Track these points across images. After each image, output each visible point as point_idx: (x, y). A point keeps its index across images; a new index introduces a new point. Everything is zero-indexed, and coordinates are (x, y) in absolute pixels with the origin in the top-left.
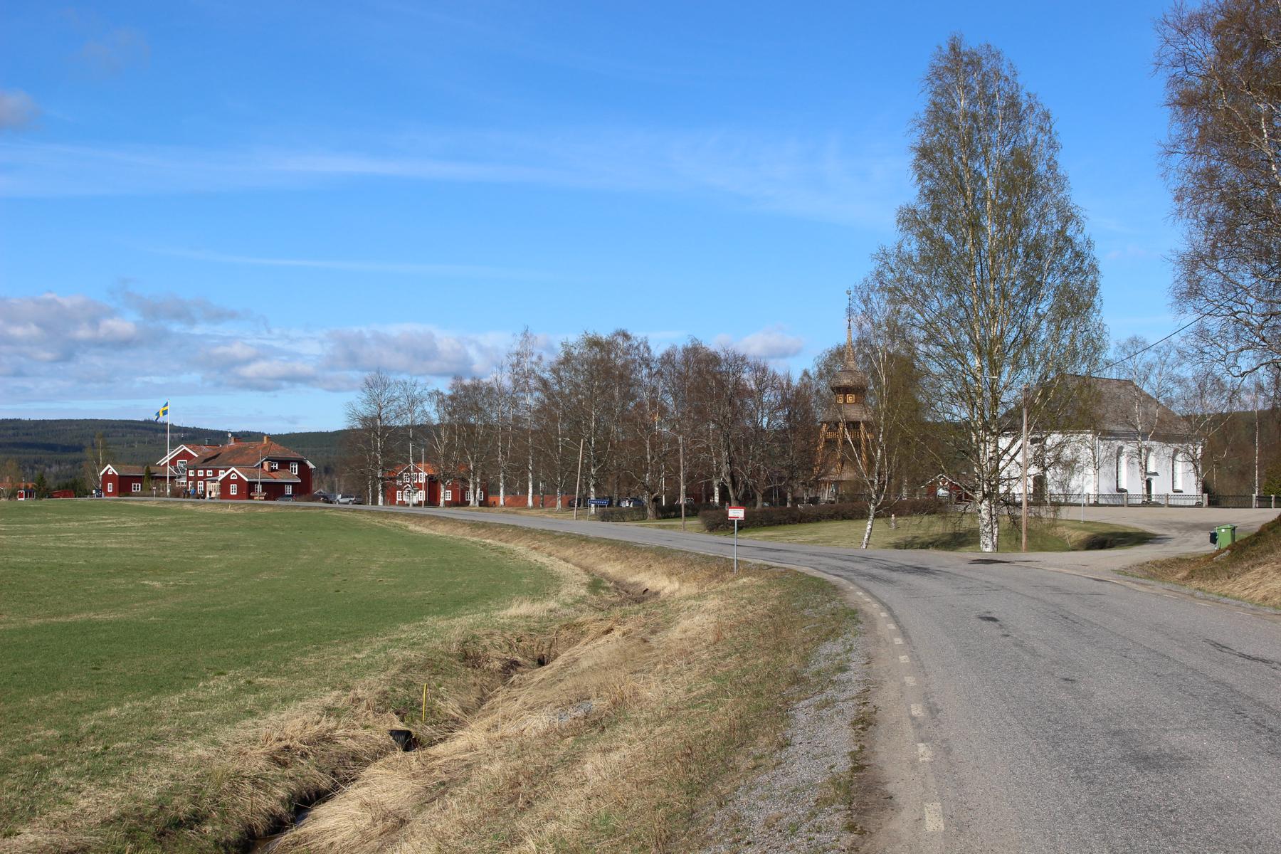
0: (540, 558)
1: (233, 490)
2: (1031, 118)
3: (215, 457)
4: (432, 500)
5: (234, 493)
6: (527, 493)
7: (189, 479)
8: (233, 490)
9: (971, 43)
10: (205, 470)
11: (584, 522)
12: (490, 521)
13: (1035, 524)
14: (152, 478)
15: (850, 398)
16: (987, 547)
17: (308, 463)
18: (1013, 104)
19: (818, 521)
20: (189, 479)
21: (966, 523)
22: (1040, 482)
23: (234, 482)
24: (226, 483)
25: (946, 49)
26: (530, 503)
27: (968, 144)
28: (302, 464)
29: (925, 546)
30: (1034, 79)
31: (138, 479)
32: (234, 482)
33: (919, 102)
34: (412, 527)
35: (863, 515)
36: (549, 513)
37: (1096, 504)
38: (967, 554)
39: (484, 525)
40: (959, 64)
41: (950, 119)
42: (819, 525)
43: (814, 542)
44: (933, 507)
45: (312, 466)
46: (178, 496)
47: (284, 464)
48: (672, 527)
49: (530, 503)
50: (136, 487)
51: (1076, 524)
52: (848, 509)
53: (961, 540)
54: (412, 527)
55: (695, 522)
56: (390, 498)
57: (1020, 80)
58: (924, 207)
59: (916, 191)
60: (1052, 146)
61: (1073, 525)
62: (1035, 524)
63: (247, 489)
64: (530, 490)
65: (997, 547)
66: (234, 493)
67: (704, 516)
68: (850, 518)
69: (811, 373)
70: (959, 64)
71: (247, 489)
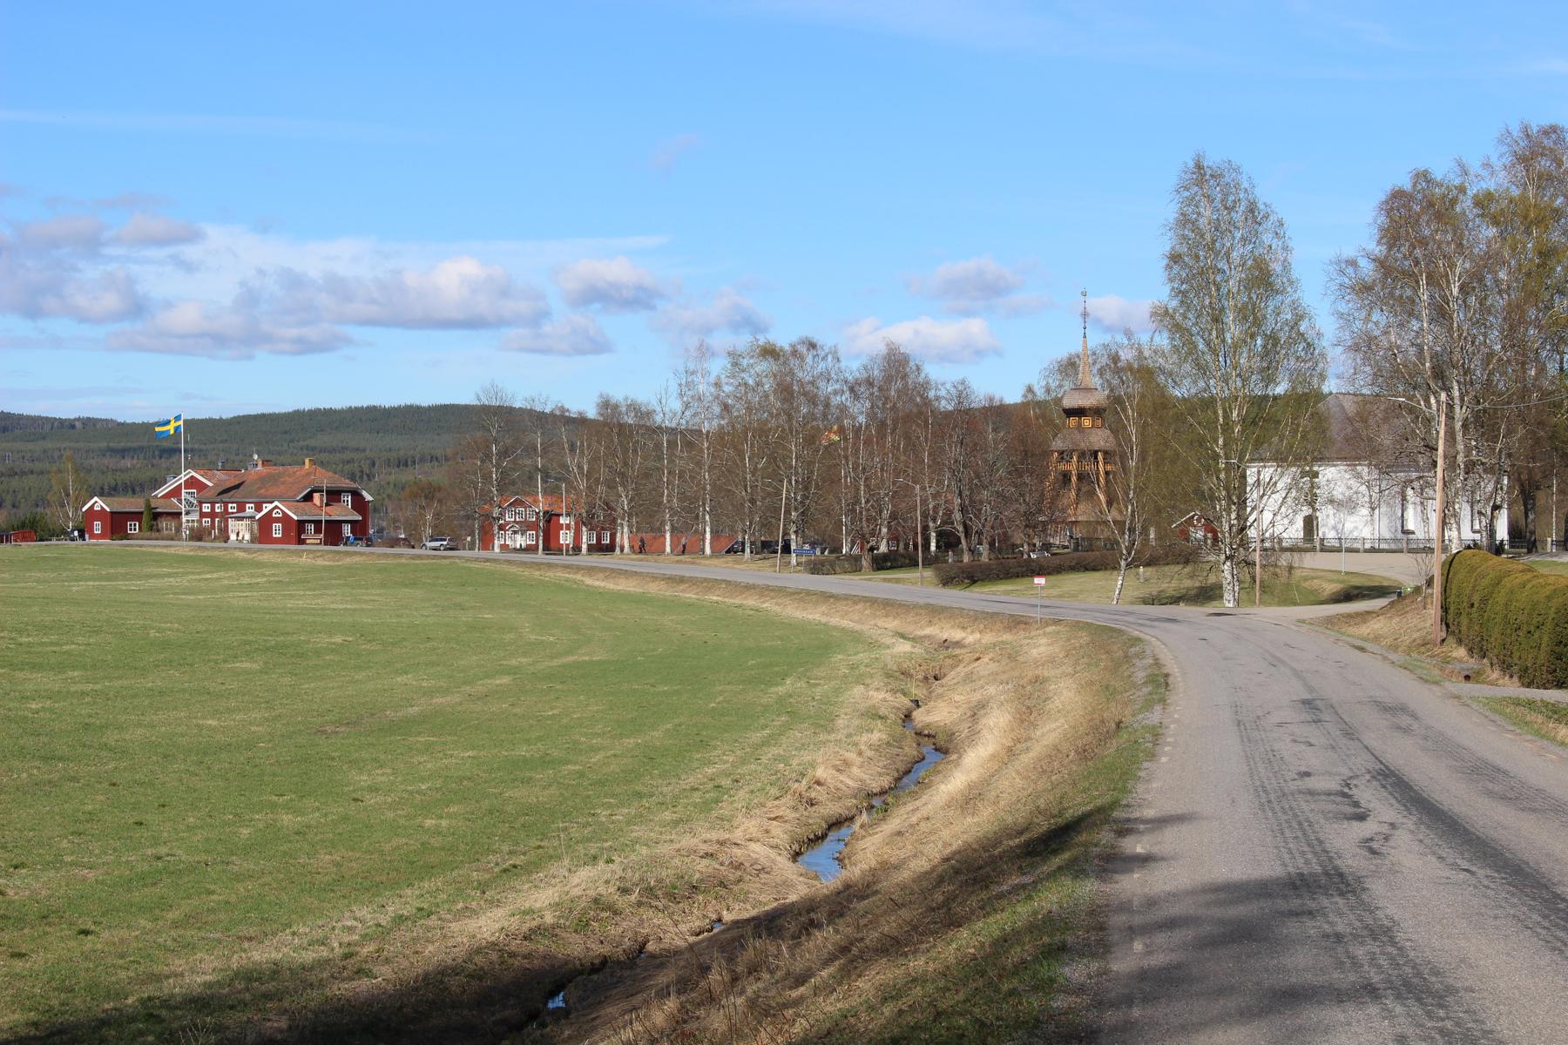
0: (814, 615)
1: (277, 531)
2: (1268, 224)
3: (237, 487)
4: (550, 545)
5: (277, 534)
6: (704, 540)
7: (203, 515)
8: (277, 531)
9: (1212, 160)
10: (213, 504)
11: (786, 575)
12: (687, 575)
13: (1271, 576)
14: (154, 519)
15: (1087, 422)
16: (1228, 602)
17: (364, 493)
18: (1252, 209)
19: (1059, 572)
20: (203, 515)
21: (1212, 579)
22: (1310, 524)
23: (277, 520)
24: (266, 522)
25: (1191, 164)
26: (708, 550)
27: (1211, 247)
28: (356, 494)
29: (1175, 600)
30: (1269, 188)
31: (136, 516)
32: (277, 520)
33: (1168, 210)
34: (588, 581)
35: (1116, 567)
36: (737, 562)
37: (1373, 550)
38: (1210, 608)
39: (682, 580)
40: (1200, 174)
41: (1196, 229)
42: (1060, 577)
43: (1060, 596)
44: (1188, 557)
45: (368, 497)
46: (200, 539)
47: (334, 495)
48: (898, 581)
49: (708, 550)
50: (133, 528)
51: (1318, 574)
52: (1090, 557)
53: (1208, 594)
54: (588, 581)
55: (928, 573)
56: (487, 543)
57: (1258, 192)
58: (1175, 303)
59: (1166, 290)
60: (1286, 248)
61: (1335, 577)
62: (1271, 576)
63: (296, 532)
64: (708, 536)
65: (1238, 602)
66: (277, 534)
67: (937, 569)
68: (1095, 569)
69: (1036, 388)
70: (1200, 174)
71: (296, 532)
